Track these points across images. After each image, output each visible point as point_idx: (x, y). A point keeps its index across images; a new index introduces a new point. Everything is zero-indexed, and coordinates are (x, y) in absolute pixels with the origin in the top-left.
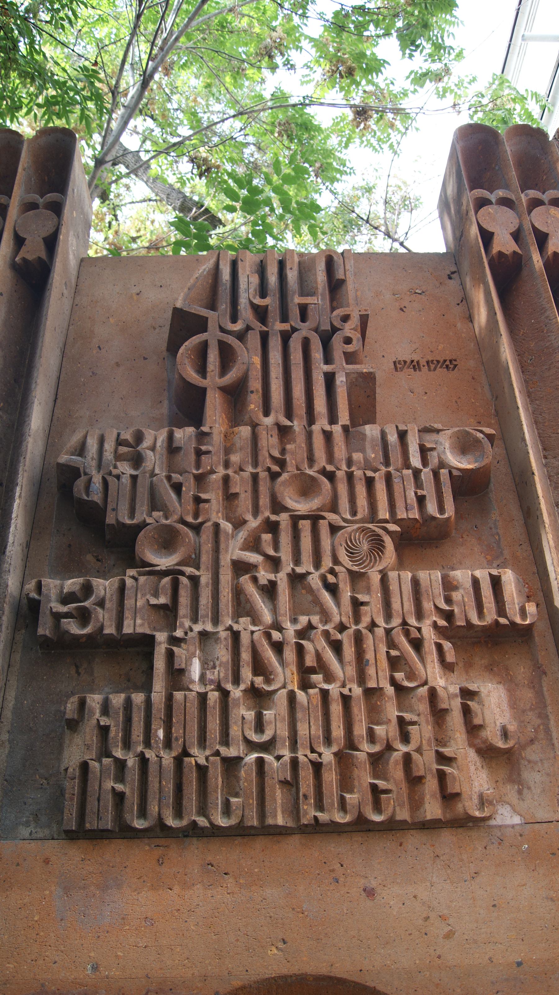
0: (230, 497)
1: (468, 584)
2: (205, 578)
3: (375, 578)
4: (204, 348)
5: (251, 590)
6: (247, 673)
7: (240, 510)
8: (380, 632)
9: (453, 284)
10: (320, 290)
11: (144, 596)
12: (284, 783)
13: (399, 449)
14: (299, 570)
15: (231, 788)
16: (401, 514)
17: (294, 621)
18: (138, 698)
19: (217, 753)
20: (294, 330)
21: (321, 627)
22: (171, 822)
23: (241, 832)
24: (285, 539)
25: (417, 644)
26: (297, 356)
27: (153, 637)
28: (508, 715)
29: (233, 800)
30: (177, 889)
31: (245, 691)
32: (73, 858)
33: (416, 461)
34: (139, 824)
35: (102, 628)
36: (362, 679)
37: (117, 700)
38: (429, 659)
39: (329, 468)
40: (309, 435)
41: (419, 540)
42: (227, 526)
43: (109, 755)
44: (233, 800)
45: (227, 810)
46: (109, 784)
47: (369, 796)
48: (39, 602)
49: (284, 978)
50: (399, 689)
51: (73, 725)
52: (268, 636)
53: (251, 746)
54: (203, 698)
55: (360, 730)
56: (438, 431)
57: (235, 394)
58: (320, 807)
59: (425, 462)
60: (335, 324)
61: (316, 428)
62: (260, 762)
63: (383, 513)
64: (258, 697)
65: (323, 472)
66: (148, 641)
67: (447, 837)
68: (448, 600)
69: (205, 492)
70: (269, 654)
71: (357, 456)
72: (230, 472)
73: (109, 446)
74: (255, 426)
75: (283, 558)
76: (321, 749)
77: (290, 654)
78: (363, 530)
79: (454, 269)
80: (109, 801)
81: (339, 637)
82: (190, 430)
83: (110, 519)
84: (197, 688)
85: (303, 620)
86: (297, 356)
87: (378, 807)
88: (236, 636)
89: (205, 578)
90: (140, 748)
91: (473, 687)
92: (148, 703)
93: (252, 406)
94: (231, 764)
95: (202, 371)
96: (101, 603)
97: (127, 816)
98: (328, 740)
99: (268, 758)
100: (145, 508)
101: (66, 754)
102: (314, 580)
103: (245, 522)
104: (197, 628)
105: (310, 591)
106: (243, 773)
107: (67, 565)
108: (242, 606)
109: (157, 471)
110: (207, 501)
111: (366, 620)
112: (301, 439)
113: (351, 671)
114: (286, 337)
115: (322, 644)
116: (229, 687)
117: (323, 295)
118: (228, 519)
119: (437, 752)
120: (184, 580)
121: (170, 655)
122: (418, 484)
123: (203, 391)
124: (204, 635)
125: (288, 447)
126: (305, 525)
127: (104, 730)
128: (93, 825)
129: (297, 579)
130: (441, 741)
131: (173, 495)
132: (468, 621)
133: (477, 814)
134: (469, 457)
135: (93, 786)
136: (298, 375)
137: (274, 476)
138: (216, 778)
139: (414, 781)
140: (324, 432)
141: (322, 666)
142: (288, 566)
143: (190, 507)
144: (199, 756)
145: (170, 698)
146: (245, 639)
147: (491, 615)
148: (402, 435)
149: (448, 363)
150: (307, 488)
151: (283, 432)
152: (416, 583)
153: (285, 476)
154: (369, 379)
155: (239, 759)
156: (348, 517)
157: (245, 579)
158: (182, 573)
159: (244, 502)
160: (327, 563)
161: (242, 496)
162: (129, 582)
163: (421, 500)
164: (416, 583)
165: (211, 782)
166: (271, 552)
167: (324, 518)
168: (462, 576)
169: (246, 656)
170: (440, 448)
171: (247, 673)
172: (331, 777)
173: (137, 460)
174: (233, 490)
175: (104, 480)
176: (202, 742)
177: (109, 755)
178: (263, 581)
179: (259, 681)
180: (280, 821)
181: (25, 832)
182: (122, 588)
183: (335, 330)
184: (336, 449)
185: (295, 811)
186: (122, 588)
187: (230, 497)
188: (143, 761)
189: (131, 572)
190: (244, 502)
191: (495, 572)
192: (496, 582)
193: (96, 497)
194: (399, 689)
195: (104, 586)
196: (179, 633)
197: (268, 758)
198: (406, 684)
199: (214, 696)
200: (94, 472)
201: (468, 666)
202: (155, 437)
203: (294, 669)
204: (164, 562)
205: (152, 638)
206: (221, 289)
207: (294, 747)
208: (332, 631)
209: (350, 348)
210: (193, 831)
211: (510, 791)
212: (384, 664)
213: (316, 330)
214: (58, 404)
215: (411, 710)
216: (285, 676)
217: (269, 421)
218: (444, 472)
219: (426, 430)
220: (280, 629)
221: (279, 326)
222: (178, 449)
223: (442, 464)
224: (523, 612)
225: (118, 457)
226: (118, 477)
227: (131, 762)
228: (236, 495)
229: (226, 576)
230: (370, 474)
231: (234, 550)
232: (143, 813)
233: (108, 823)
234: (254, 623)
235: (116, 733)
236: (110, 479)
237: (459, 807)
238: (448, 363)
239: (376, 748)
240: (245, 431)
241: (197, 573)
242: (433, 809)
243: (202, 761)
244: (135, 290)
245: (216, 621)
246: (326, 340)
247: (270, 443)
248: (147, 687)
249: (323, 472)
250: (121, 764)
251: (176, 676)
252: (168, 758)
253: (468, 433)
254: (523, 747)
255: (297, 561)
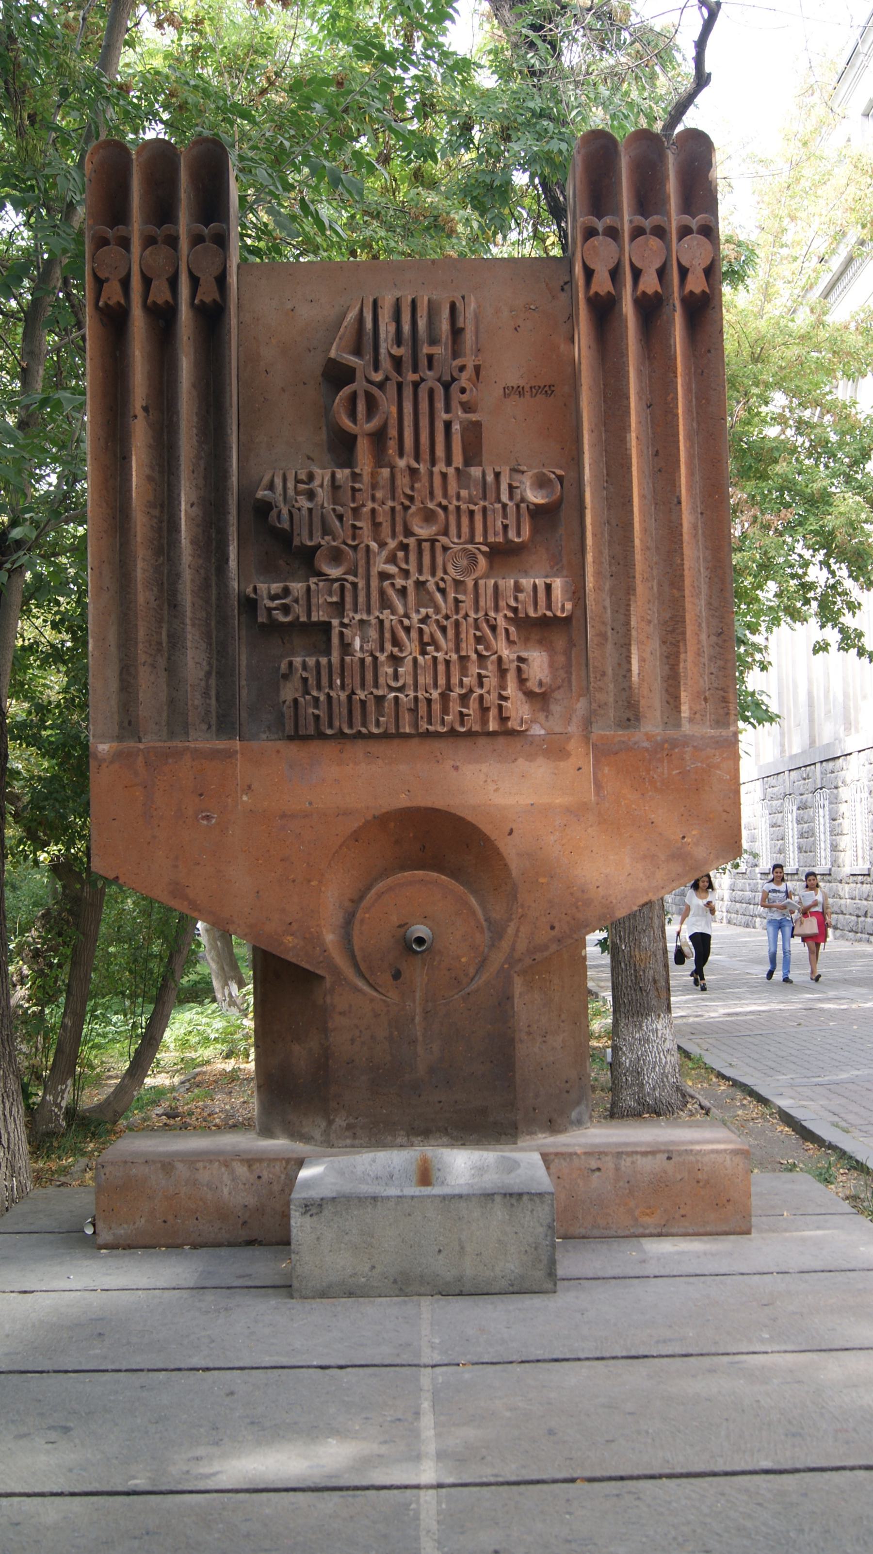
0: (376, 526)
1: (530, 588)
2: (361, 584)
3: (470, 584)
4: (353, 397)
5: (391, 592)
6: (388, 646)
7: (383, 535)
8: (471, 620)
9: (563, 297)
10: (444, 340)
11: (324, 598)
12: (410, 710)
13: (494, 486)
14: (422, 579)
15: (380, 712)
16: (491, 539)
17: (418, 612)
18: (324, 661)
19: (372, 693)
20: (422, 380)
21: (434, 617)
22: (347, 731)
23: (386, 736)
24: (413, 557)
25: (493, 628)
26: (424, 406)
27: (330, 623)
28: (546, 671)
29: (381, 719)
30: (351, 765)
31: (387, 657)
32: (292, 750)
33: (505, 498)
34: (329, 732)
35: (298, 617)
36: (458, 650)
37: (311, 661)
38: (499, 639)
39: (444, 502)
40: (431, 474)
41: (503, 554)
42: (374, 545)
43: (309, 694)
44: (381, 719)
45: (378, 724)
46: (311, 710)
47: (458, 718)
48: (256, 600)
49: (409, 808)
50: (480, 656)
51: (286, 677)
52: (401, 622)
53: (391, 689)
54: (362, 661)
55: (455, 680)
56: (523, 472)
57: (379, 438)
58: (430, 723)
59: (511, 497)
60: (454, 374)
61: (436, 470)
62: (396, 698)
63: (479, 538)
64: (395, 660)
65: (439, 505)
66: (326, 627)
67: (501, 740)
68: (516, 599)
69: (360, 520)
70: (402, 634)
71: (464, 493)
72: (376, 507)
73: (290, 484)
74: (393, 468)
75: (412, 570)
76: (432, 691)
77: (414, 634)
78: (465, 550)
79: (567, 279)
80: (311, 719)
81: (445, 623)
82: (347, 471)
83: (296, 542)
84: (359, 655)
85: (423, 611)
86: (424, 406)
87: (462, 724)
88: (381, 622)
89: (361, 584)
90: (327, 690)
91: (524, 654)
92: (330, 662)
93: (391, 451)
94: (380, 699)
95: (353, 415)
96: (296, 601)
97: (322, 728)
98: (436, 686)
99: (401, 695)
100: (319, 533)
101: (282, 693)
102: (431, 586)
103: (386, 544)
104: (358, 617)
105: (428, 592)
106: (386, 704)
107: (269, 570)
108: (385, 603)
109: (326, 505)
110: (361, 528)
111: (462, 613)
112: (425, 479)
113: (451, 645)
114: (416, 385)
115: (435, 627)
116: (378, 654)
117: (446, 344)
118: (375, 541)
119: (500, 694)
120: (348, 585)
121: (341, 634)
122: (505, 516)
123: (354, 437)
124: (361, 621)
125: (416, 485)
126: (426, 546)
127: (305, 680)
128: (304, 730)
129: (420, 585)
130: (503, 687)
131: (338, 523)
132: (527, 614)
133: (519, 728)
134: (544, 492)
135: (301, 711)
136: (424, 422)
137: (406, 508)
138: (371, 707)
139: (484, 710)
140: (442, 473)
141: (434, 642)
142: (415, 576)
143: (350, 533)
144: (361, 695)
145: (342, 661)
146: (387, 624)
147: (542, 610)
148: (497, 475)
149: (547, 388)
150: (429, 517)
151: (413, 472)
152: (496, 586)
153: (413, 508)
154: (477, 426)
155: (384, 697)
156: (456, 540)
157: (387, 583)
158: (346, 580)
159: (386, 529)
160: (440, 573)
161: (384, 524)
162: (313, 587)
163: (505, 527)
164: (496, 586)
165: (368, 709)
166: (404, 566)
167: (438, 541)
168: (526, 583)
169: (387, 635)
170: (523, 487)
171: (388, 646)
172: (437, 707)
173: (311, 495)
174: (378, 520)
175: (290, 511)
176: (363, 686)
177: (309, 694)
178: (398, 587)
179: (395, 650)
180: (407, 730)
181: (264, 736)
182: (308, 589)
183: (454, 380)
184: (449, 487)
185: (416, 725)
186: (308, 589)
187: (376, 526)
188: (329, 697)
189: (315, 580)
190: (386, 529)
191: (548, 581)
192: (548, 587)
193: (286, 525)
194: (480, 656)
195: (297, 587)
196: (346, 621)
197: (401, 695)
198: (485, 653)
199: (369, 660)
200: (282, 505)
201: (527, 640)
202: (322, 475)
203: (417, 643)
204: (335, 572)
205: (329, 624)
206: (365, 338)
207: (416, 690)
208: (441, 620)
209: (464, 398)
210: (359, 735)
211: (541, 716)
212: (472, 640)
213: (439, 380)
214: (241, 430)
215: (486, 669)
216: (411, 647)
217: (402, 463)
218: (523, 505)
219: (514, 470)
220: (409, 618)
221: (411, 377)
222: (339, 487)
223: (523, 500)
224: (563, 609)
225: (297, 493)
226: (299, 509)
227: (322, 698)
228: (380, 524)
229: (374, 583)
230: (472, 507)
231: (380, 565)
232: (331, 726)
233: (311, 731)
234: (393, 613)
235: (312, 681)
236: (294, 511)
237: (510, 724)
238: (547, 388)
239: (464, 691)
240: (385, 472)
241: (356, 580)
242: (492, 726)
243: (363, 698)
244: (289, 306)
245: (369, 612)
246: (447, 386)
247: (403, 481)
248: (328, 652)
249: (439, 505)
250: (316, 700)
251: (346, 647)
252: (343, 696)
253: (544, 474)
254: (553, 691)
255: (420, 572)
